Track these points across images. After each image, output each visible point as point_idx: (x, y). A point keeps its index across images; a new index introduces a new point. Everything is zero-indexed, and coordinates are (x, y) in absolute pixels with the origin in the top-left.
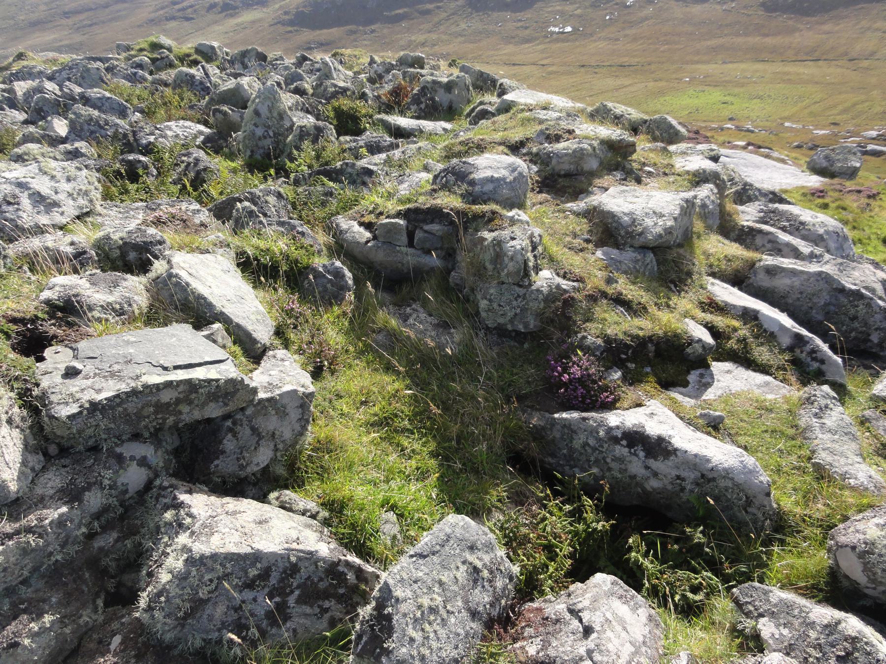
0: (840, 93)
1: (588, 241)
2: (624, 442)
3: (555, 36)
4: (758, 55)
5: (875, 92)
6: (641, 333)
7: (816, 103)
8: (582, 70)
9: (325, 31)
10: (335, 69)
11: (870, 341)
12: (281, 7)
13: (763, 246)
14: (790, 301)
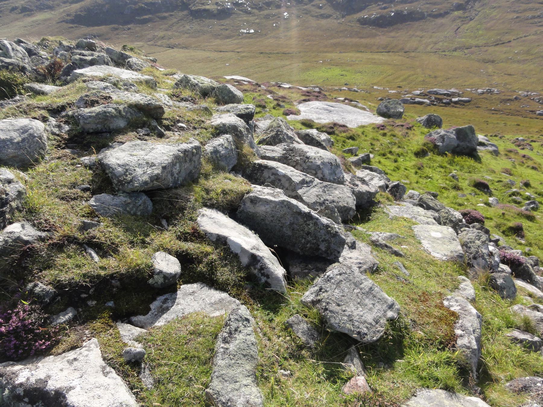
0: (401, 70)
1: (85, 190)
2: (26, 400)
3: (244, 35)
4: (358, 48)
5: (418, 70)
6: (103, 273)
7: (389, 75)
8: (262, 55)
9: (96, 28)
10: (13, 49)
11: (320, 249)
12: (64, 11)
13: (269, 177)
14: (267, 222)
